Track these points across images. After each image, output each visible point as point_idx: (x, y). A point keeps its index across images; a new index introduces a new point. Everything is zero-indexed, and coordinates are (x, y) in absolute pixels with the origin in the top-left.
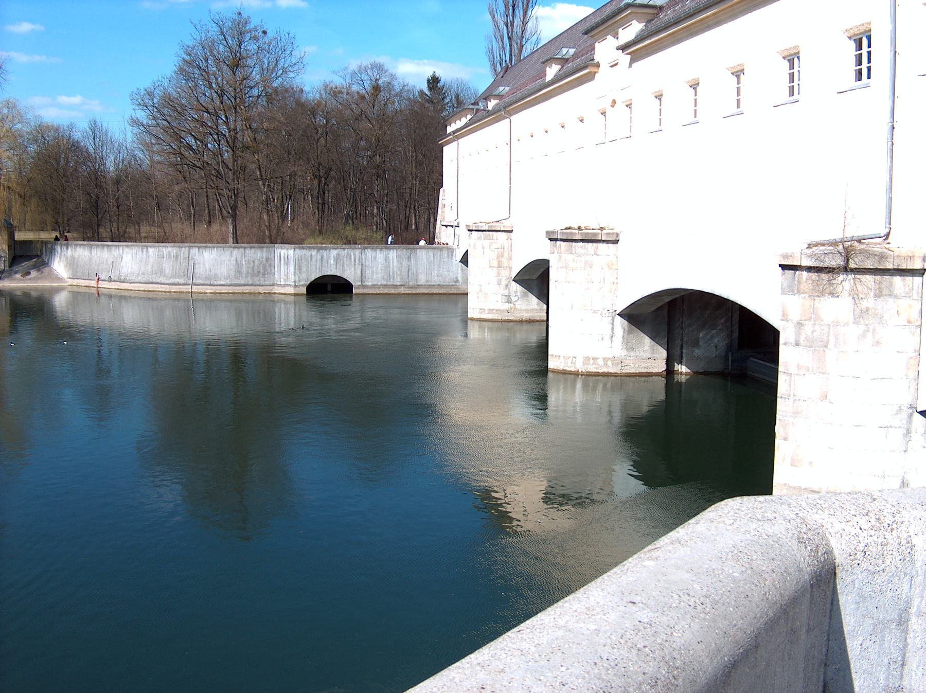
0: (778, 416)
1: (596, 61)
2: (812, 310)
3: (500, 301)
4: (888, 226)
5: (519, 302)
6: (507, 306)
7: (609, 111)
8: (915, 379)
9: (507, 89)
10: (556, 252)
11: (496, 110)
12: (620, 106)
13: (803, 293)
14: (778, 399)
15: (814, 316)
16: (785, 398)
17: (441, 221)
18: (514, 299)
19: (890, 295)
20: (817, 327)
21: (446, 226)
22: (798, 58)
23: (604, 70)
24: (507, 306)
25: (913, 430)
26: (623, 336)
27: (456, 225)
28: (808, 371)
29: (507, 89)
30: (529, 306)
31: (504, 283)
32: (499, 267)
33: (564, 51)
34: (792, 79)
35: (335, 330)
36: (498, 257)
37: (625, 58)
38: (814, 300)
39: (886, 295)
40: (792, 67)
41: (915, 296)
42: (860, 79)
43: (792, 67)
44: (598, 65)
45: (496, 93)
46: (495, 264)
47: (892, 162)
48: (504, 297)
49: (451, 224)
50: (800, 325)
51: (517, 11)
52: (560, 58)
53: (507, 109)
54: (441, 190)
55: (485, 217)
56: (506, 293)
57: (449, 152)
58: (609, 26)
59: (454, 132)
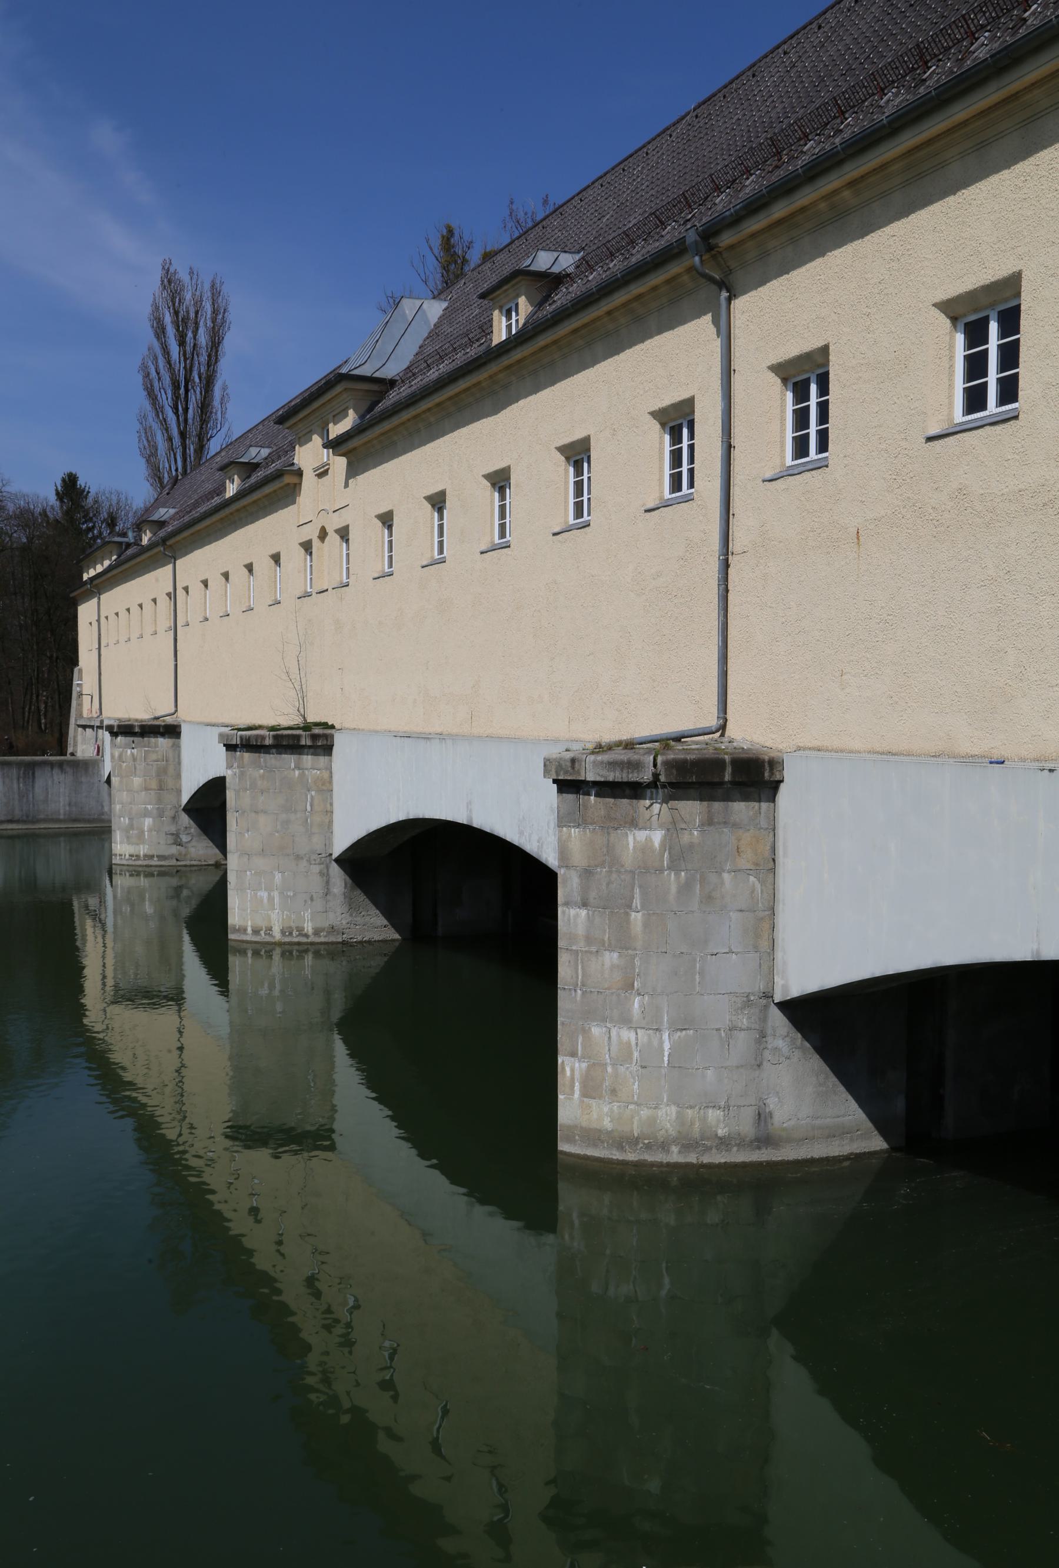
0: (560, 1019)
1: (295, 468)
2: (605, 850)
3: (162, 842)
4: (722, 715)
5: (194, 843)
6: (174, 850)
7: (316, 543)
8: (769, 953)
9: (172, 511)
10: (235, 765)
11: (152, 546)
12: (333, 538)
13: (591, 824)
14: (559, 991)
15: (610, 858)
16: (570, 989)
17: (76, 720)
18: (184, 838)
19: (725, 823)
20: (614, 876)
21: (84, 727)
22: (589, 457)
23: (309, 479)
24: (174, 850)
25: (769, 1031)
26: (344, 894)
27: (99, 725)
28: (603, 945)
29: (172, 511)
30: (201, 849)
31: (169, 813)
32: (161, 789)
33: (253, 451)
34: (579, 491)
35: (662, 747)
36: (158, 775)
37: (339, 464)
38: (609, 833)
39: (719, 823)
40: (579, 472)
41: (764, 823)
42: (680, 489)
43: (579, 472)
44: (299, 473)
45: (155, 517)
46: (154, 784)
47: (176, 660)
48: (169, 836)
49: (92, 724)
50: (587, 873)
51: (191, 394)
52: (245, 463)
53: (168, 543)
54: (76, 670)
55: (139, 713)
56: (173, 829)
57: (86, 612)
58: (315, 410)
59: (92, 579)
